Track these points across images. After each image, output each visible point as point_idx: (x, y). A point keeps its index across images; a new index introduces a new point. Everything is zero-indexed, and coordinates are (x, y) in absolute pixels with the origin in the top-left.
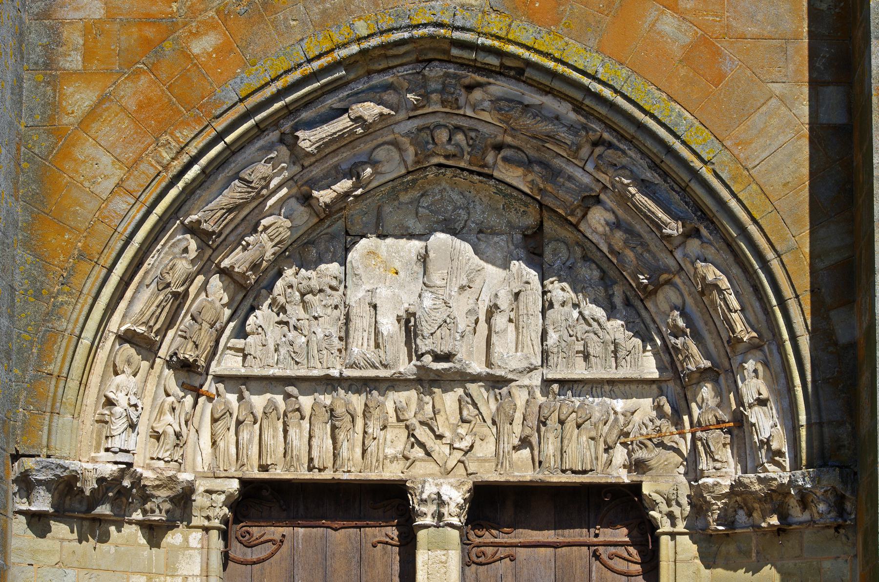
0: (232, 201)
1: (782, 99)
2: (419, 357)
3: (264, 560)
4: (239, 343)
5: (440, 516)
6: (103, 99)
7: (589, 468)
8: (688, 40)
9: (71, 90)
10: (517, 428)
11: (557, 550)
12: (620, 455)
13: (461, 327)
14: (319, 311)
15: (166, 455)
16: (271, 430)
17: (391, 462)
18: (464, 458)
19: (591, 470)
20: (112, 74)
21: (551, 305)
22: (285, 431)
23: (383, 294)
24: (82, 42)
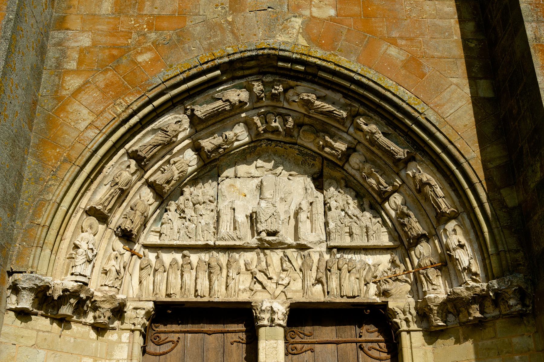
0: (156, 141)
1: (457, 85)
2: (259, 233)
3: (167, 353)
4: (158, 228)
5: (272, 320)
6: (87, 82)
7: (357, 295)
8: (404, 58)
9: (69, 78)
10: (314, 274)
11: (338, 345)
12: (373, 289)
13: (282, 218)
14: (203, 212)
15: (110, 283)
16: (174, 275)
17: (243, 292)
18: (284, 290)
19: (358, 296)
20: (92, 70)
21: (330, 209)
22: (182, 275)
23: (238, 204)
24: (77, 57)
